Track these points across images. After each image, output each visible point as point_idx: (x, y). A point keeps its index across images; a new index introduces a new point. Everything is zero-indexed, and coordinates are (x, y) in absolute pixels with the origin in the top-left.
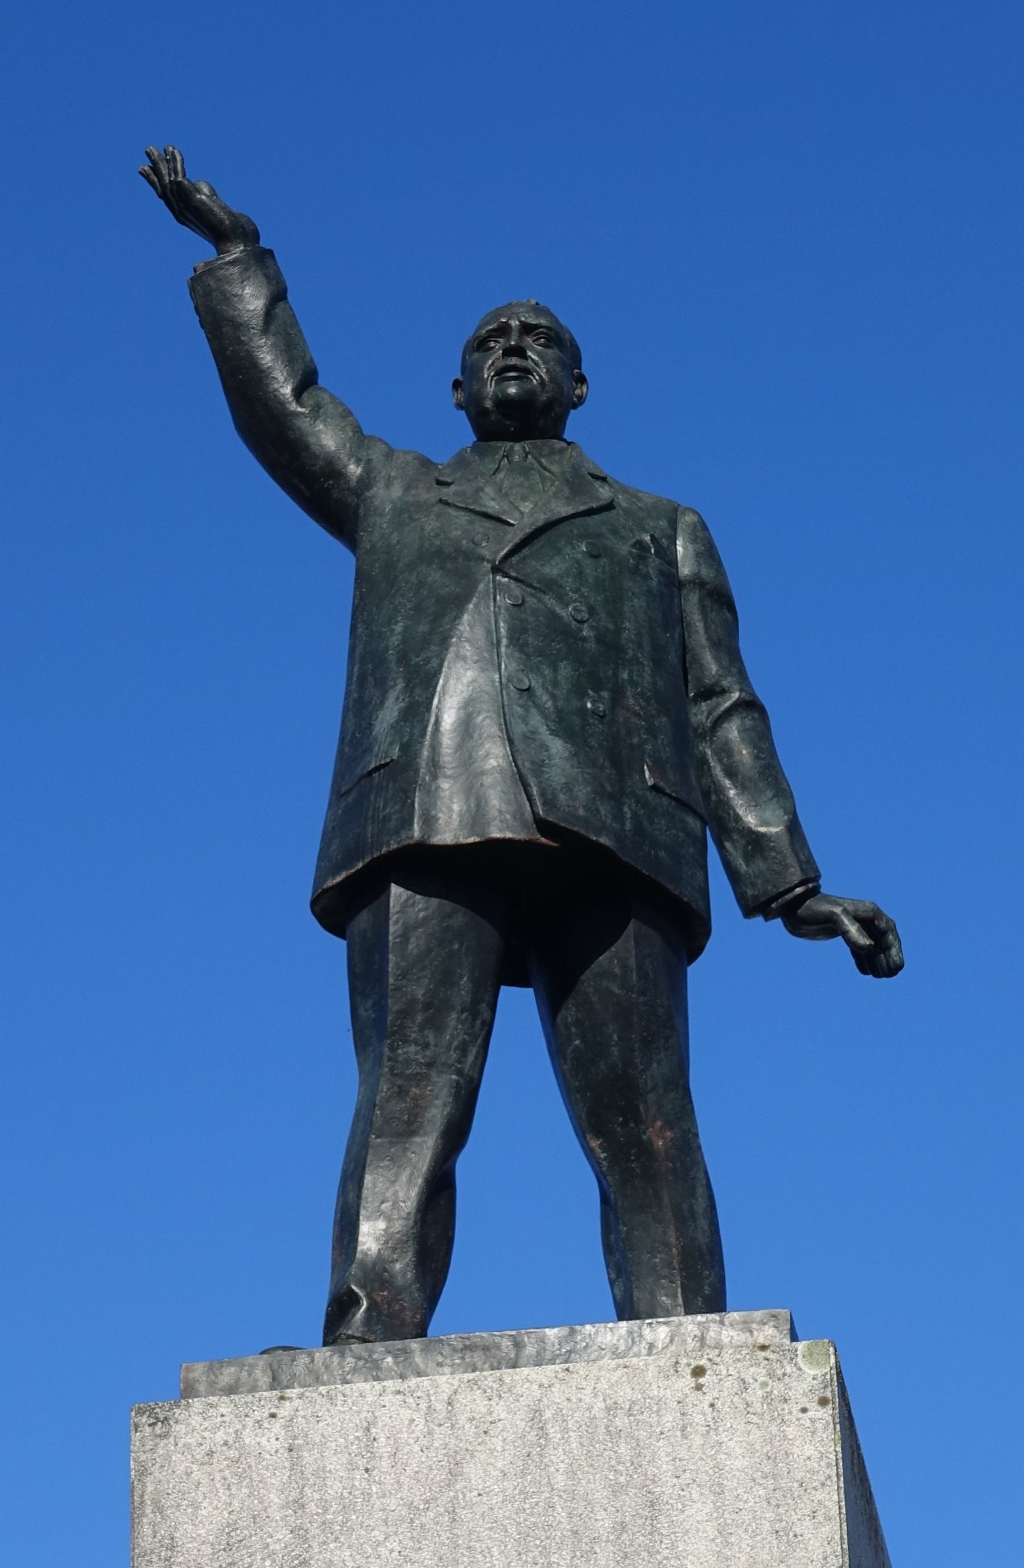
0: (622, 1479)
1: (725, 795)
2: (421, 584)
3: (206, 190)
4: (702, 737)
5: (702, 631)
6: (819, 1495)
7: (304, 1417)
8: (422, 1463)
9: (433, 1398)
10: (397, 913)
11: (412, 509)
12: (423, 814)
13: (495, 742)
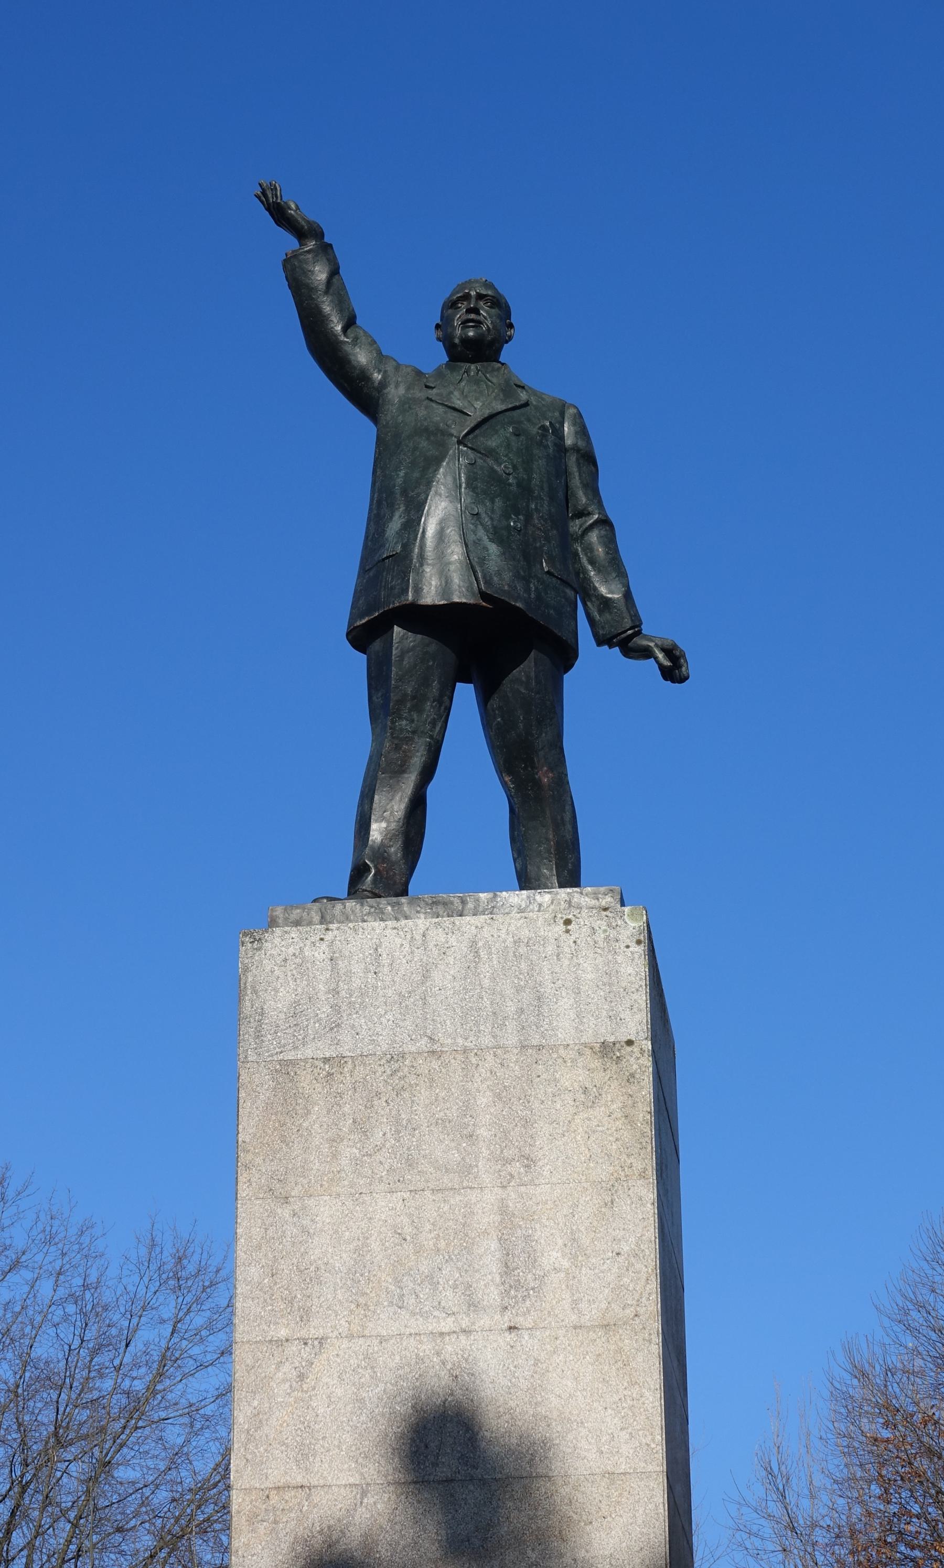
0: (522, 983)
1: (588, 575)
2: (415, 449)
3: (293, 206)
4: (576, 540)
5: (577, 478)
6: (635, 996)
7: (340, 941)
8: (407, 970)
9: (414, 932)
10: (397, 643)
11: (411, 402)
12: (415, 586)
13: (457, 545)
